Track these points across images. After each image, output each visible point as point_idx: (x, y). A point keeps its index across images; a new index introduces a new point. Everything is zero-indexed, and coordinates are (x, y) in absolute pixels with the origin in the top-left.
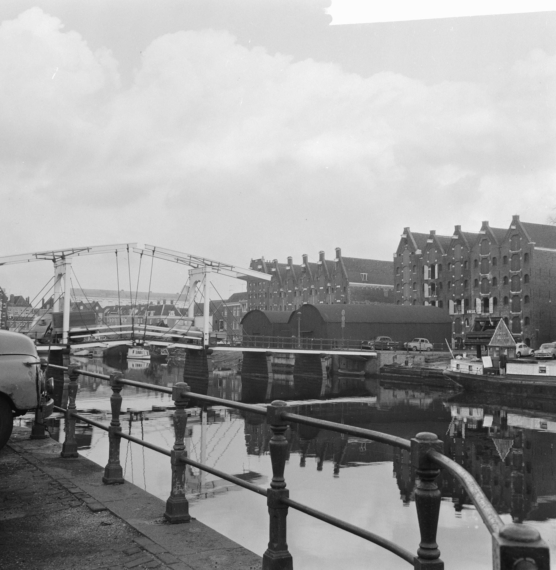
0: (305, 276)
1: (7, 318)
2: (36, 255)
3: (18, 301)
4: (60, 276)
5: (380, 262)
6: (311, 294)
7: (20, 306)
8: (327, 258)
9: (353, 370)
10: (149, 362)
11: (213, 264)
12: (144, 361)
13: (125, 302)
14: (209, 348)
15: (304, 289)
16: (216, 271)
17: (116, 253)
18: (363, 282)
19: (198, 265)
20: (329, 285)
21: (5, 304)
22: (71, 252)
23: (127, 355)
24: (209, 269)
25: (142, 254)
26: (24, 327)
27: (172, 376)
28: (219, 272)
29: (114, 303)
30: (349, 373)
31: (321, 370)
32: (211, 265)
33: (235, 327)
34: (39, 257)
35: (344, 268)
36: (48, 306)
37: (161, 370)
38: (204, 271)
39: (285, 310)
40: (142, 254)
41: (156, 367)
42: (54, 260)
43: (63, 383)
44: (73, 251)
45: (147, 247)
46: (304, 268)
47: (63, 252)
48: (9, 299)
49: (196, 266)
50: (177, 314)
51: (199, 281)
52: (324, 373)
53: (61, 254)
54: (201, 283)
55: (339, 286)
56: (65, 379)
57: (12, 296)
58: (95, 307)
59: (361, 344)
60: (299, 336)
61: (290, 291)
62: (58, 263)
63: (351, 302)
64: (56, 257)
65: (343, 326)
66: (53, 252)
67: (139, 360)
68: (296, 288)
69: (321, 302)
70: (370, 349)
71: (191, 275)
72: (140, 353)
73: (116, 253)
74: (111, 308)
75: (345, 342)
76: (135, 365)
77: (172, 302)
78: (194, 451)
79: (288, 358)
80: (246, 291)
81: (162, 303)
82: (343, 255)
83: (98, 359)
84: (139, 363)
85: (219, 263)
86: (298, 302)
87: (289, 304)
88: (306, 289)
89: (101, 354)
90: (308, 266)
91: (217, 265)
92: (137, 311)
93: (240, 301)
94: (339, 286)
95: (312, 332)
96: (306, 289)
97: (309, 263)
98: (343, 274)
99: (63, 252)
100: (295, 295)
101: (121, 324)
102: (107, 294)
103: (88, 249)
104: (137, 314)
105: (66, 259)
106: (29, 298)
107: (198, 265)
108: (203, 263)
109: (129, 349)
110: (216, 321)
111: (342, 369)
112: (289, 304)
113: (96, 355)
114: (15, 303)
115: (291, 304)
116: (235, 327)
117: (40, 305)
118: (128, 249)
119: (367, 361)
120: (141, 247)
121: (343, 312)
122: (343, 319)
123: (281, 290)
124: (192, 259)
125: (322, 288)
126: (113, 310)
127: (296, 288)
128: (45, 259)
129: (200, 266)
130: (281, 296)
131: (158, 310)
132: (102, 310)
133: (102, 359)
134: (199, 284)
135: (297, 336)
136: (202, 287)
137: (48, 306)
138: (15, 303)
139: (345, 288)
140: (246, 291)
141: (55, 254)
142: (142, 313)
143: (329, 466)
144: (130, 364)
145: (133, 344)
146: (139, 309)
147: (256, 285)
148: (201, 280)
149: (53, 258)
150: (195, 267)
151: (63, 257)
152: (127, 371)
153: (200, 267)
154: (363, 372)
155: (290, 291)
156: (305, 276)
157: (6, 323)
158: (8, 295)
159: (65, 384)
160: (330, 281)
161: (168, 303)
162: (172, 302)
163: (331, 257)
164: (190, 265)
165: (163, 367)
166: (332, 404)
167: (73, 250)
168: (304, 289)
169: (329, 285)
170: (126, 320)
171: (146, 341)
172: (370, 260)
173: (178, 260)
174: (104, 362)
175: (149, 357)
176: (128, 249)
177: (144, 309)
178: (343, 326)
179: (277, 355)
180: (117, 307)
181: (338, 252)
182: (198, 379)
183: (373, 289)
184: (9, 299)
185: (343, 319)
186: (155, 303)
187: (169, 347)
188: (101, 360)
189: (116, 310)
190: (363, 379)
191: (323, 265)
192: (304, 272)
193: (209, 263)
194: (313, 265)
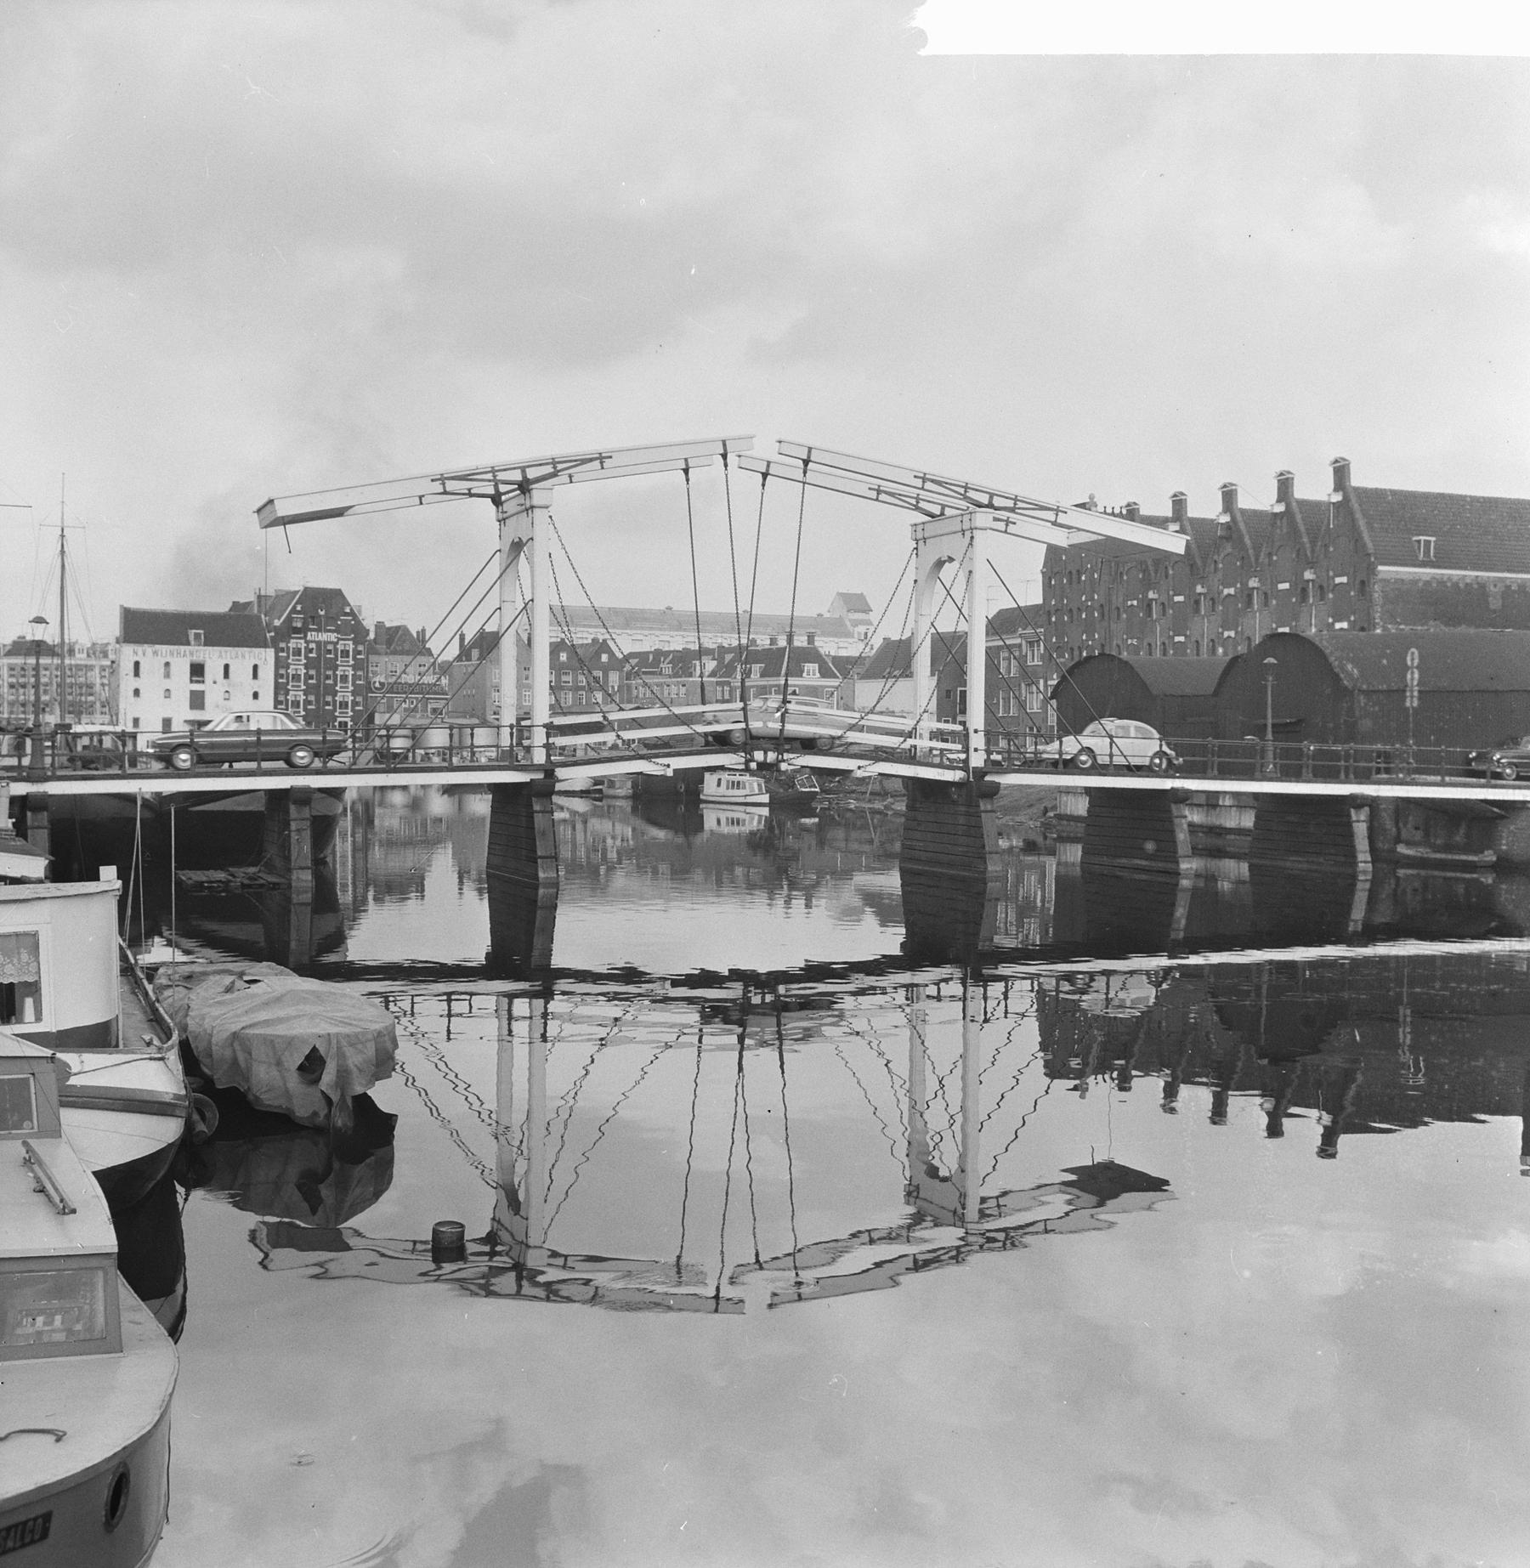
0: (1229, 549)
1: (369, 687)
2: (442, 479)
3: (396, 640)
4: (517, 547)
5: (1475, 500)
6: (1249, 602)
7: (402, 653)
8: (1303, 491)
9: (1448, 848)
10: (765, 811)
11: (997, 502)
12: (749, 809)
13: (678, 642)
14: (987, 778)
15: (1226, 591)
16: (1001, 526)
17: (686, 471)
18: (1423, 564)
19: (943, 507)
20: (1308, 575)
21: (360, 648)
22: (549, 469)
23: (698, 792)
24: (983, 518)
25: (765, 475)
26: (414, 710)
27: (828, 852)
28: (1011, 528)
29: (646, 642)
30: (1438, 856)
31: (1353, 847)
32: (990, 506)
33: (1007, 709)
34: (451, 486)
35: (1362, 523)
36: (475, 653)
37: (797, 837)
38: (966, 526)
39: (1165, 653)
40: (765, 475)
41: (781, 825)
42: (496, 500)
43: (537, 889)
44: (557, 468)
45: (786, 449)
46: (1227, 526)
47: (523, 470)
48: (372, 636)
49: (936, 510)
50: (825, 673)
51: (951, 560)
52: (1361, 857)
53: (517, 476)
54: (956, 564)
55: (1344, 580)
56: (541, 875)
57: (379, 626)
58: (598, 655)
59: (1469, 762)
60: (1270, 736)
61: (1180, 599)
62: (510, 507)
63: (1385, 629)
64: (503, 488)
65: (1412, 702)
66: (493, 471)
67: (736, 802)
68: (1199, 589)
69: (1338, 626)
70: (1498, 776)
71: (920, 540)
72: (738, 785)
73: (686, 471)
74: (642, 656)
75: (1418, 756)
76: (723, 821)
77: (811, 638)
78: (940, 1093)
79: (1215, 806)
80: (1040, 601)
81: (782, 642)
82: (1357, 480)
83: (619, 803)
84: (736, 815)
85: (1016, 500)
86: (1259, 625)
87: (1177, 639)
88: (1232, 591)
89: (625, 789)
90: (1239, 517)
91: (1010, 504)
92: (711, 665)
93: (1020, 631)
94: (1344, 580)
95: (1300, 721)
96: (1232, 591)
97: (1243, 511)
98: (1358, 540)
99: (523, 470)
100: (1197, 611)
101: (704, 703)
102: (632, 619)
103: (601, 458)
104: (713, 674)
105: (534, 493)
106: (424, 630)
107: (943, 507)
108: (965, 498)
109: (707, 775)
110: (948, 692)
111: (1408, 843)
112: (1177, 639)
113: (611, 792)
114: (389, 643)
115: (1182, 639)
116: (1007, 709)
117: (453, 651)
118: (724, 456)
119: (1502, 817)
120: (764, 449)
121: (1413, 657)
122: (1413, 677)
123: (1151, 595)
124: (928, 485)
125: (1286, 586)
126: (648, 662)
127: (1199, 589)
128: (471, 495)
129: (948, 512)
130: (1150, 614)
131: (772, 660)
132: (617, 664)
133: (630, 803)
134: (948, 571)
135: (1262, 737)
136: (962, 577)
137: (475, 653)
138: (389, 643)
139: (1363, 582)
140: (1040, 601)
141: (501, 476)
142: (729, 670)
143: (1307, 1124)
144: (710, 819)
145: (747, 762)
146: (720, 660)
147: (1070, 582)
148: (958, 556)
149: (491, 491)
150: (932, 516)
151: (524, 487)
152: (700, 839)
153: (947, 516)
154: (1489, 856)
155: (1180, 599)
156: (1229, 549)
157: (366, 699)
158: (369, 623)
159: (541, 891)
160: (1311, 565)
161: (800, 641)
162: (811, 638)
163: (1316, 488)
164: (917, 508)
165: (805, 829)
166: (1384, 961)
167: (554, 463)
168: (1226, 591)
169: (1308, 575)
170: (683, 690)
171: (786, 756)
172: (1442, 496)
173: (879, 492)
174: (634, 810)
175: (765, 799)
176: (724, 456)
177: (732, 661)
178: (1412, 702)
179: (1211, 801)
180: (659, 654)
181: (1341, 471)
182: (952, 878)
183: (1456, 585)
184: (372, 636)
185: (1413, 677)
186: (763, 642)
187: (859, 774)
188: (626, 805)
189: (656, 663)
190: (1489, 879)
191: (1288, 513)
192: (1228, 538)
193: (984, 499)
194: (1254, 516)
